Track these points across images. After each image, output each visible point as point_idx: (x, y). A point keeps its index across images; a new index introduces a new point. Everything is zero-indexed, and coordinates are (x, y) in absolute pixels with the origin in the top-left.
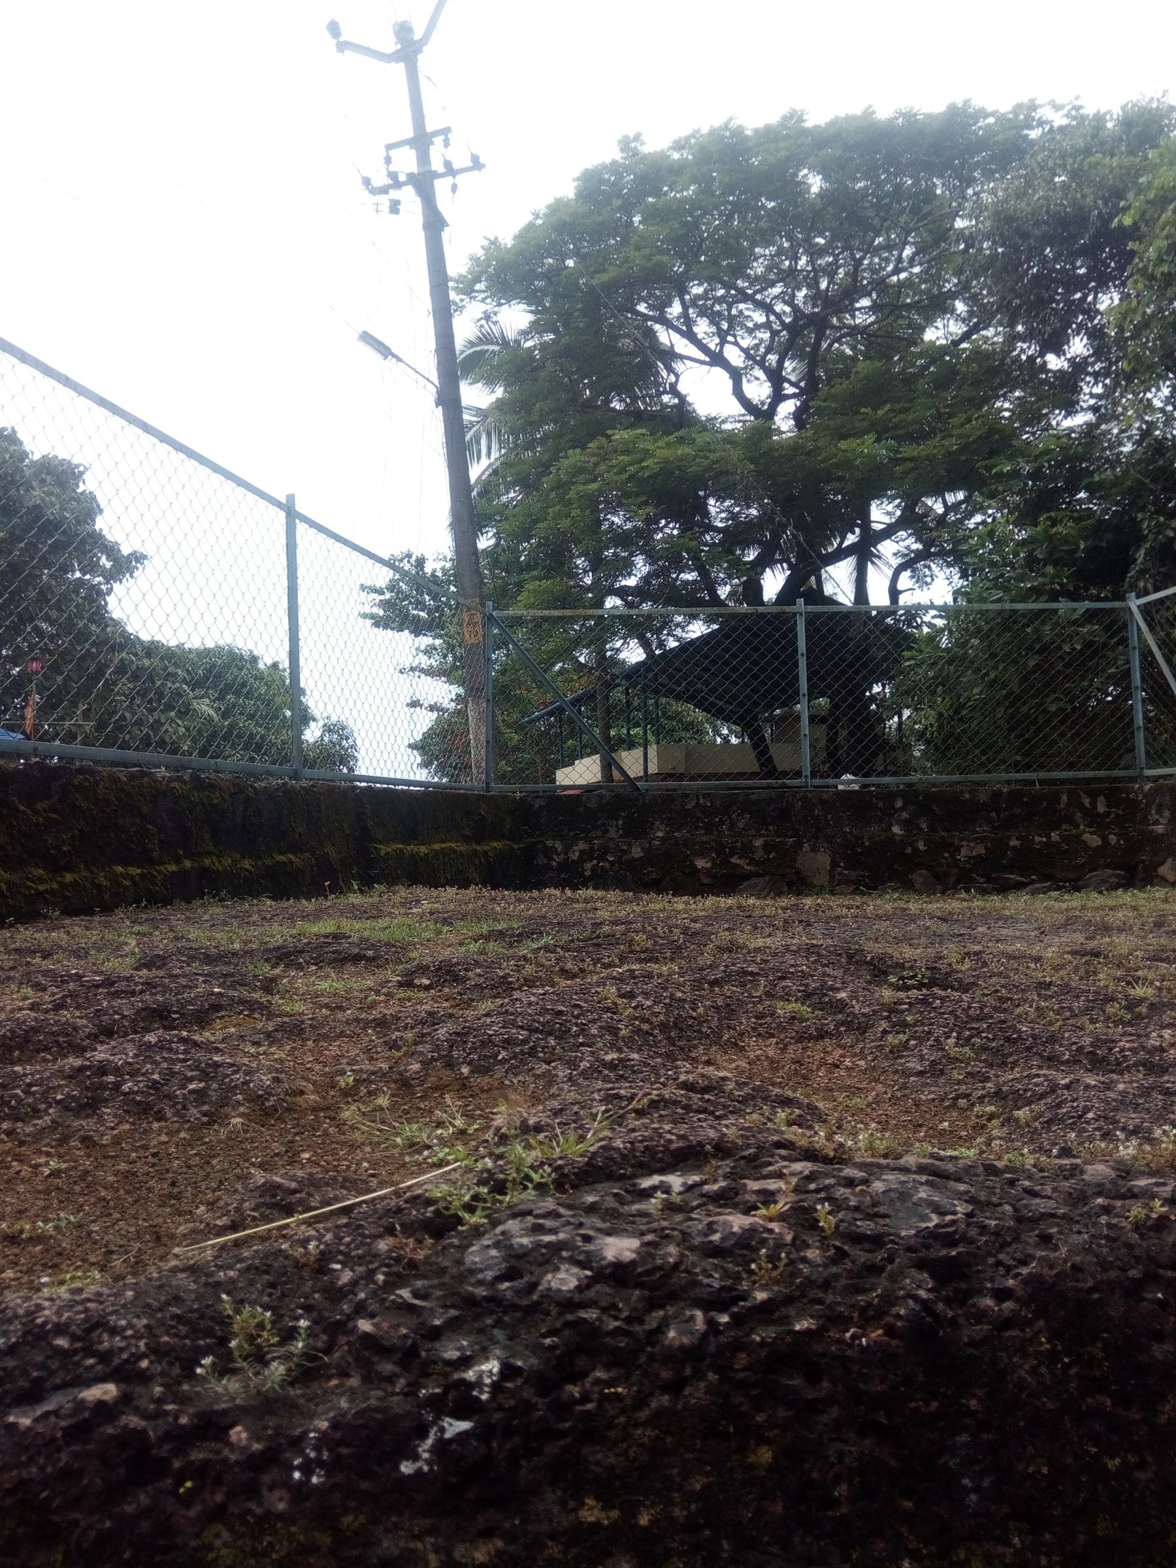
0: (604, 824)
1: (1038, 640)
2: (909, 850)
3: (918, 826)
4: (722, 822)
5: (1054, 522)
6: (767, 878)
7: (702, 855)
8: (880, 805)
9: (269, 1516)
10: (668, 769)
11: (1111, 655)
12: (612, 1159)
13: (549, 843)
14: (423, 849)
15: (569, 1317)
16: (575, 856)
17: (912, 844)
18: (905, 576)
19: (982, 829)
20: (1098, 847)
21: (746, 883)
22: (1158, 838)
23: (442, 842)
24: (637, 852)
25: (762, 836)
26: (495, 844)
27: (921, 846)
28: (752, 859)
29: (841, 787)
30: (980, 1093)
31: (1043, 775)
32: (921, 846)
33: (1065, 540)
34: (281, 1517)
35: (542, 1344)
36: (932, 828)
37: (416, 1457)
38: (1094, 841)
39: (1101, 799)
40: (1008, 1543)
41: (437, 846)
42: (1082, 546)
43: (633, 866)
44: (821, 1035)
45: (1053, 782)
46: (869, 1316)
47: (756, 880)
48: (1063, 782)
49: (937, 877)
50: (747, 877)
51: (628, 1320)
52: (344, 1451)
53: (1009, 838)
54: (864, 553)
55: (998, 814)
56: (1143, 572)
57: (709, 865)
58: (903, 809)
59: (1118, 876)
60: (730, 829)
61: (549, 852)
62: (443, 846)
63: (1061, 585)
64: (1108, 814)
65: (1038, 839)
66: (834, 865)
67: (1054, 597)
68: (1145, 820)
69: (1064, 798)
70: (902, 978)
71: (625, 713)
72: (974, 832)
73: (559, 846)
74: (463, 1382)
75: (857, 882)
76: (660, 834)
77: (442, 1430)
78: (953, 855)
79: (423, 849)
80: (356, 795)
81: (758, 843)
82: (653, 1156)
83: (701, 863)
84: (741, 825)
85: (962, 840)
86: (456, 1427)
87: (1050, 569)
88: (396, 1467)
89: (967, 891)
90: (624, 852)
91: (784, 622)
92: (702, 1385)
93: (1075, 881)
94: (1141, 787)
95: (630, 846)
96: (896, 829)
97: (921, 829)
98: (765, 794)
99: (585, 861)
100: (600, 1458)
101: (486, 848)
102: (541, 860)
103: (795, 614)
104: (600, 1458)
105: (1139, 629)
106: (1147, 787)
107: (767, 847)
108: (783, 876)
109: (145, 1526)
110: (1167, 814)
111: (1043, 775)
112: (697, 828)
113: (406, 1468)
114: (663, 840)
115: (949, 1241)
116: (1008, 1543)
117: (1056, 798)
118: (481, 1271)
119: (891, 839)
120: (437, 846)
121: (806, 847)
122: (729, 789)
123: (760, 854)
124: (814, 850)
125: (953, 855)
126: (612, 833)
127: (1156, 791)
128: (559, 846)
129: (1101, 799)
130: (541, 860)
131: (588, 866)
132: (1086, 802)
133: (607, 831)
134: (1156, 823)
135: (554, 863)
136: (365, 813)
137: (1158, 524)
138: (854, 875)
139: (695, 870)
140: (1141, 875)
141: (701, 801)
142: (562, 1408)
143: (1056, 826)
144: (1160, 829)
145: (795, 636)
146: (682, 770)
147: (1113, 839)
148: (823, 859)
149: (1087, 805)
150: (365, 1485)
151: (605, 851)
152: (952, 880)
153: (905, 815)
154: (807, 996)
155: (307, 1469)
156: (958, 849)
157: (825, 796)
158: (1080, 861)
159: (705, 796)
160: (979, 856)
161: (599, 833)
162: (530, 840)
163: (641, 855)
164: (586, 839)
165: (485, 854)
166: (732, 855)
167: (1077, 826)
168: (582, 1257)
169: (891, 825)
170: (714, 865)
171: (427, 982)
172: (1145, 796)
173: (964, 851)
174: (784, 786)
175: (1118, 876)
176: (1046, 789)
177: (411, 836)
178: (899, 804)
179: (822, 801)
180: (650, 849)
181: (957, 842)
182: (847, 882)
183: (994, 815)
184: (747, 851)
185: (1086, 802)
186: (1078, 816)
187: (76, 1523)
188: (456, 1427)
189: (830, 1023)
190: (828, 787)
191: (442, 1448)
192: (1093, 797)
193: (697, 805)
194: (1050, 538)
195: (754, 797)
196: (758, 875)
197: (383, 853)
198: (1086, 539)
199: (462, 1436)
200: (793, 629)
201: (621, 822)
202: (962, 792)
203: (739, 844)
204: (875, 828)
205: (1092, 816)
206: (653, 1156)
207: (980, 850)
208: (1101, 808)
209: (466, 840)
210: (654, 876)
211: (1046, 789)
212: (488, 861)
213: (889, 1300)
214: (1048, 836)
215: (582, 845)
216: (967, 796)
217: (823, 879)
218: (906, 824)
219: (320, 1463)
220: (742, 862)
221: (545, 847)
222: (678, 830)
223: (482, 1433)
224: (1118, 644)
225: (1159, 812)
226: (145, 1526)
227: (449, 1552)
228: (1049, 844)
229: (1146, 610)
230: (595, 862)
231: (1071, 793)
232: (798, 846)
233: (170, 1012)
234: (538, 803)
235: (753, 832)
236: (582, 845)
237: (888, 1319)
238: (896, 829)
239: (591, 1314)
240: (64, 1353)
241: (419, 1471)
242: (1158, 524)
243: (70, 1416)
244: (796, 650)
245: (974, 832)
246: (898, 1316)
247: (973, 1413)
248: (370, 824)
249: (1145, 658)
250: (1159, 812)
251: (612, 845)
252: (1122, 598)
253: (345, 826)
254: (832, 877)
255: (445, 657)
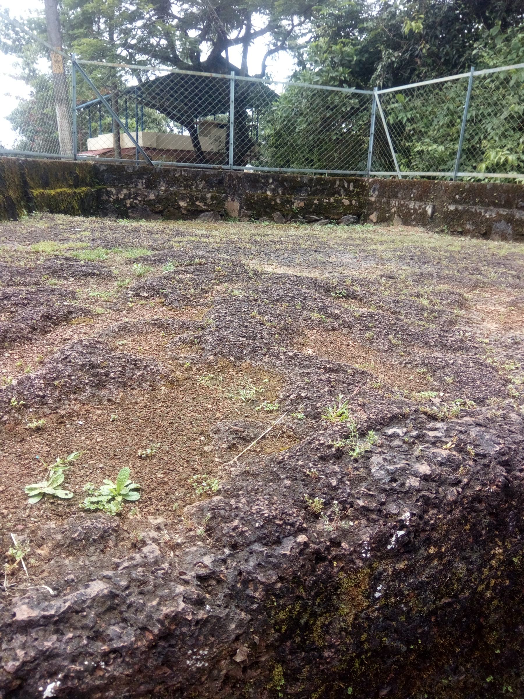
0: (136, 181)
1: (332, 103)
2: (273, 203)
3: (278, 192)
4: (192, 185)
5: (345, 45)
6: (212, 212)
7: (183, 199)
8: (263, 181)
9: (358, 568)
10: (148, 145)
11: (361, 114)
12: (372, 423)
13: (109, 189)
14: (52, 192)
15: (420, 494)
16: (122, 196)
17: (275, 200)
18: (269, 58)
19: (304, 195)
20: (348, 205)
21: (202, 214)
22: (371, 203)
23: (60, 187)
24: (152, 197)
25: (210, 192)
26: (84, 189)
27: (278, 201)
28: (206, 203)
29: (245, 171)
30: (416, 363)
31: (330, 171)
32: (278, 201)
33: (348, 55)
34: (361, 568)
35: (417, 505)
36: (283, 193)
37: (391, 544)
38: (346, 202)
39: (352, 184)
40: (516, 538)
41: (59, 190)
42: (355, 59)
43: (150, 203)
44: (334, 329)
45: (336, 175)
46: (492, 482)
47: (206, 213)
48: (338, 175)
49: (284, 216)
50: (203, 211)
51: (436, 493)
52: (374, 545)
53: (314, 199)
54: (246, 40)
55: (311, 188)
56: (379, 76)
57: (186, 205)
58: (272, 183)
59: (354, 218)
60: (196, 188)
61: (109, 193)
62: (61, 190)
63: (345, 77)
64: (354, 190)
65: (325, 200)
66: (241, 208)
67: (341, 85)
68: (367, 195)
69: (338, 183)
70: (336, 294)
71: (124, 111)
72: (301, 196)
73: (114, 191)
74: (401, 520)
75: (251, 216)
76: (163, 188)
77: (397, 535)
78: (291, 206)
79: (52, 192)
80: (20, 164)
81: (209, 195)
82: (384, 420)
83: (182, 204)
84: (201, 186)
85: (295, 199)
86: (401, 533)
87: (341, 69)
88: (386, 548)
89: (296, 222)
90: (146, 196)
91: (225, 83)
92: (458, 510)
93: (338, 219)
94: (368, 180)
95: (149, 193)
96: (268, 193)
97: (279, 194)
98: (212, 172)
99: (127, 199)
100: (435, 535)
101: (80, 191)
102: (105, 198)
103: (230, 80)
104: (435, 535)
105: (377, 105)
106: (371, 180)
107: (212, 198)
108: (219, 212)
109: (324, 577)
110: (377, 193)
111: (330, 171)
112: (181, 186)
113: (389, 547)
114: (165, 191)
115: (503, 454)
116: (516, 538)
117: (333, 182)
118: (383, 479)
119: (266, 198)
120: (59, 190)
121: (229, 199)
122: (195, 168)
123: (209, 201)
124: (233, 200)
125: (291, 206)
126: (140, 186)
127: (374, 182)
128: (114, 191)
129: (352, 184)
130: (105, 198)
131: (128, 202)
132: (346, 185)
133: (137, 185)
134: (372, 196)
135: (111, 199)
136: (25, 173)
137: (389, 54)
138: (249, 213)
139: (180, 207)
140: (362, 218)
141: (183, 173)
142: (427, 523)
143: (333, 195)
144: (373, 199)
145: (229, 92)
146: (154, 146)
147: (354, 202)
148: (236, 205)
149: (346, 186)
150: (378, 554)
151: (136, 195)
152: (289, 217)
153: (273, 186)
154: (320, 310)
155: (366, 553)
156: (293, 203)
157: (239, 175)
158: (341, 211)
159: (184, 171)
160: (301, 207)
161: (133, 186)
162: (99, 187)
163: (154, 198)
164: (127, 188)
165: (80, 194)
166: (197, 200)
167: (341, 196)
168: (413, 473)
169: (266, 191)
170: (188, 205)
171: (147, 295)
172: (369, 184)
173: (295, 205)
174: (221, 168)
175: (354, 218)
176: (331, 178)
177: (46, 185)
178: (271, 181)
179: (238, 177)
180: (158, 195)
181: (293, 200)
182: (246, 216)
183: (309, 188)
184: (203, 199)
185: (346, 185)
186: (342, 191)
187: (306, 580)
188: (401, 533)
189: (336, 324)
190: (240, 170)
191: (397, 540)
192: (349, 182)
193: (181, 175)
194: (342, 52)
195: (207, 173)
196: (208, 211)
197: (35, 195)
198: (357, 55)
199: (402, 536)
200: (228, 87)
201: (144, 181)
202: (297, 177)
203: (200, 196)
204: (260, 192)
205: (348, 192)
206: (384, 420)
207: (302, 204)
208: (351, 188)
209: (70, 186)
210: (160, 209)
211: (331, 178)
212: (81, 198)
213: (496, 477)
214: (329, 199)
215: (125, 191)
216: (299, 179)
217: (235, 214)
218: (274, 191)
219: (368, 550)
220: (201, 205)
221: (107, 191)
222: (172, 187)
223: (408, 534)
224: (364, 109)
225: (374, 192)
226: (324, 577)
227: (394, 567)
228: (329, 203)
229: (379, 96)
230: (132, 200)
231: (341, 180)
232: (226, 197)
233: (52, 316)
234: (102, 168)
235: (206, 190)
236: (125, 191)
237: (496, 483)
238: (268, 193)
239: (426, 493)
240: (279, 526)
241: (392, 548)
242: (389, 54)
243: (298, 548)
244: (229, 99)
245: (301, 196)
246: (499, 481)
247: (514, 506)
248: (28, 179)
249: (378, 120)
250: (374, 192)
251: (140, 192)
252: (372, 90)
253: (16, 180)
254: (240, 213)
255: (24, 69)
